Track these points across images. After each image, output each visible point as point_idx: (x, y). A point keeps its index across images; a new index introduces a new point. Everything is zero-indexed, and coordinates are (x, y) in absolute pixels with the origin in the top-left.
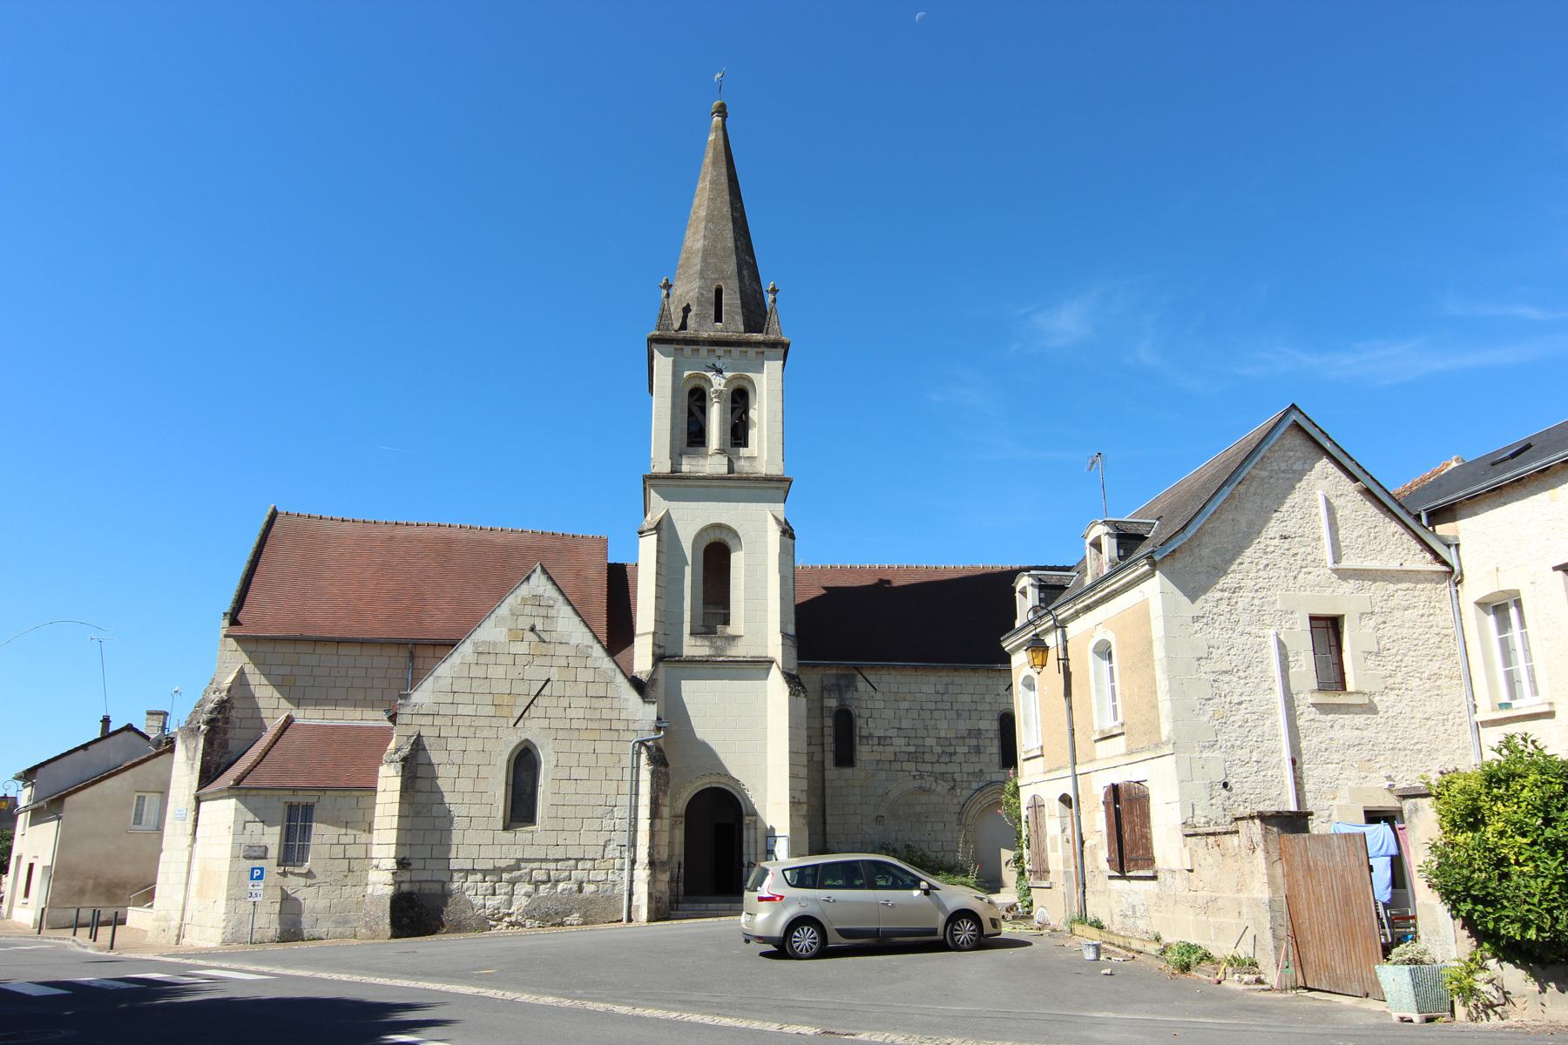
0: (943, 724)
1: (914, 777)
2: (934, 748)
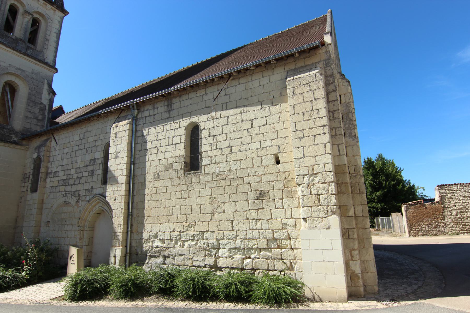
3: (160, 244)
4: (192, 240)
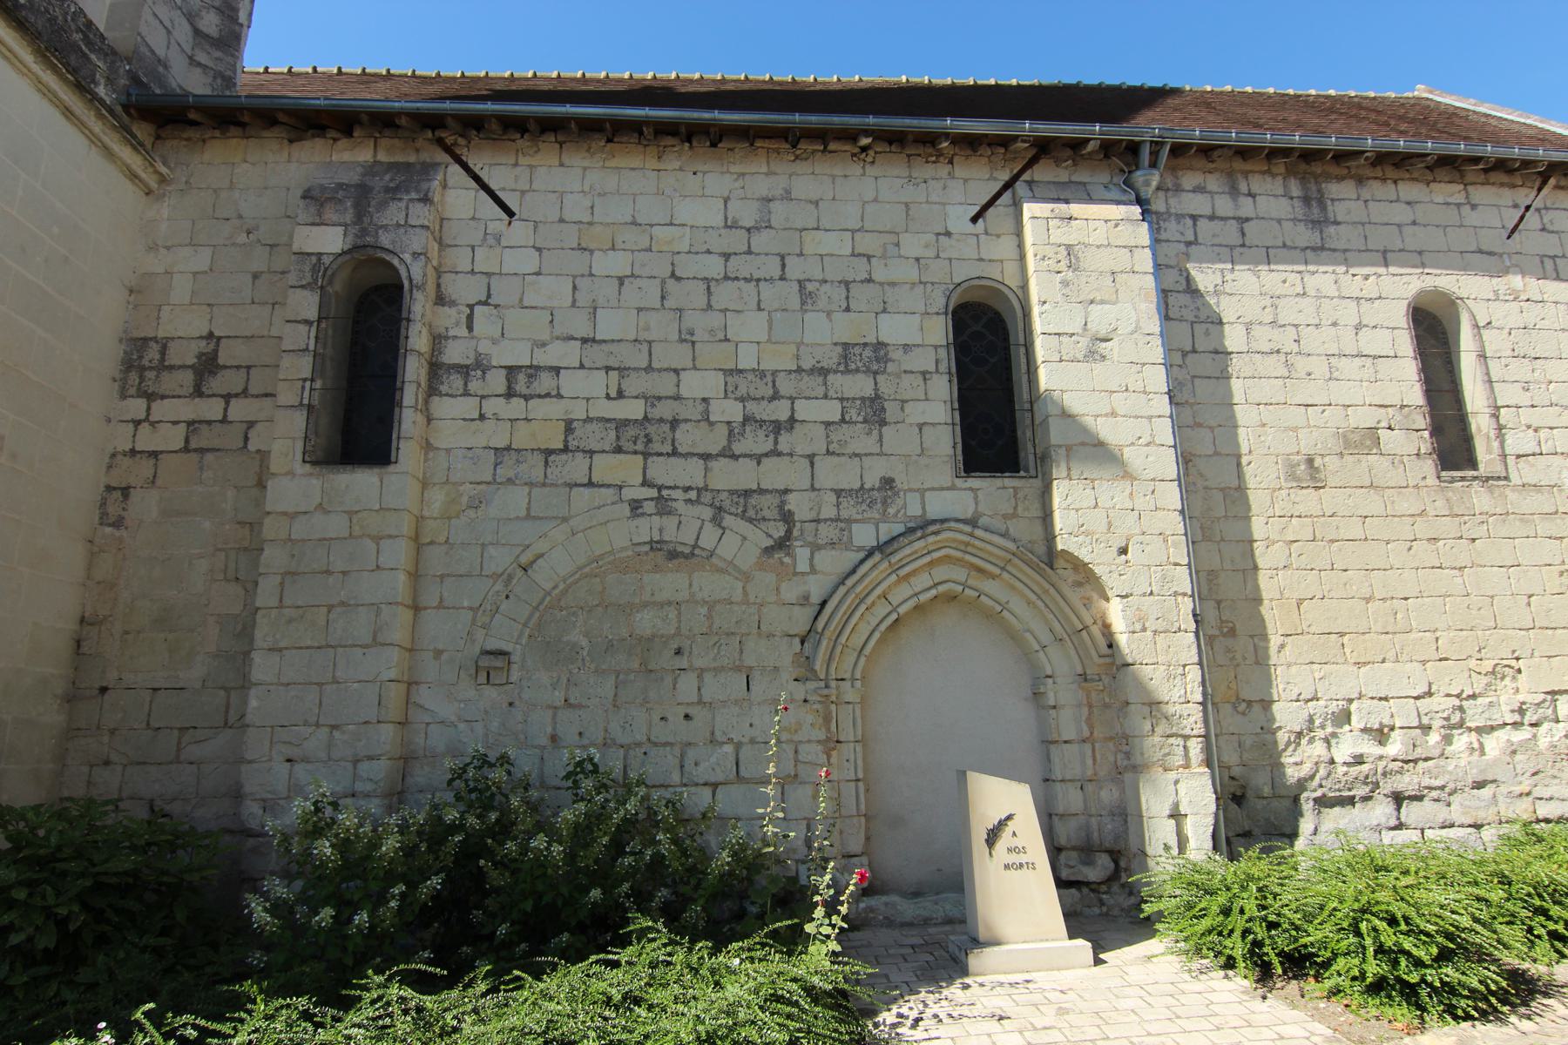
0: (750, 327)
1: (635, 506)
2: (715, 407)
3: (1369, 748)
4: (1516, 725)
